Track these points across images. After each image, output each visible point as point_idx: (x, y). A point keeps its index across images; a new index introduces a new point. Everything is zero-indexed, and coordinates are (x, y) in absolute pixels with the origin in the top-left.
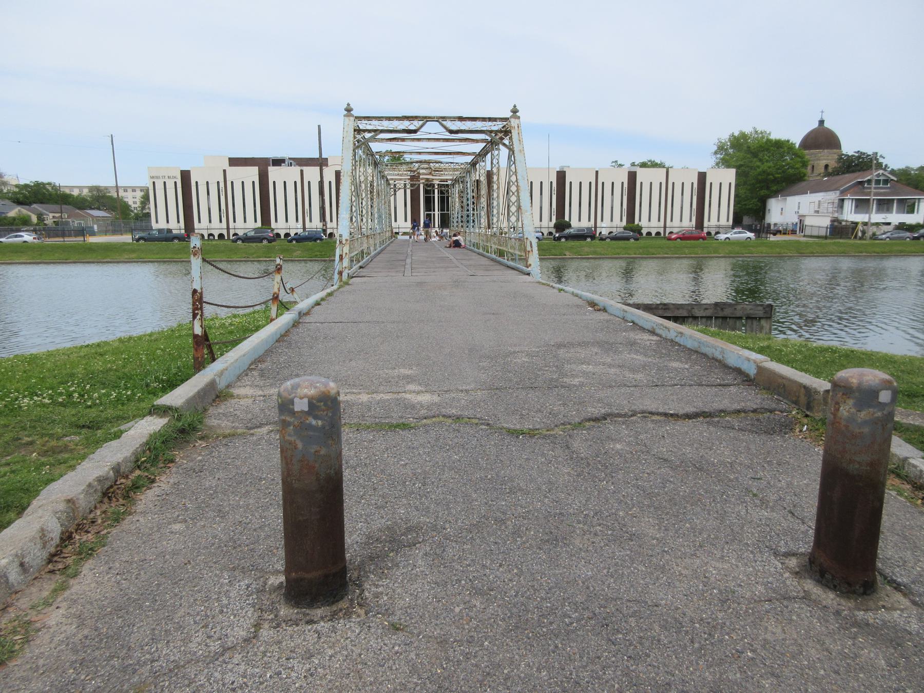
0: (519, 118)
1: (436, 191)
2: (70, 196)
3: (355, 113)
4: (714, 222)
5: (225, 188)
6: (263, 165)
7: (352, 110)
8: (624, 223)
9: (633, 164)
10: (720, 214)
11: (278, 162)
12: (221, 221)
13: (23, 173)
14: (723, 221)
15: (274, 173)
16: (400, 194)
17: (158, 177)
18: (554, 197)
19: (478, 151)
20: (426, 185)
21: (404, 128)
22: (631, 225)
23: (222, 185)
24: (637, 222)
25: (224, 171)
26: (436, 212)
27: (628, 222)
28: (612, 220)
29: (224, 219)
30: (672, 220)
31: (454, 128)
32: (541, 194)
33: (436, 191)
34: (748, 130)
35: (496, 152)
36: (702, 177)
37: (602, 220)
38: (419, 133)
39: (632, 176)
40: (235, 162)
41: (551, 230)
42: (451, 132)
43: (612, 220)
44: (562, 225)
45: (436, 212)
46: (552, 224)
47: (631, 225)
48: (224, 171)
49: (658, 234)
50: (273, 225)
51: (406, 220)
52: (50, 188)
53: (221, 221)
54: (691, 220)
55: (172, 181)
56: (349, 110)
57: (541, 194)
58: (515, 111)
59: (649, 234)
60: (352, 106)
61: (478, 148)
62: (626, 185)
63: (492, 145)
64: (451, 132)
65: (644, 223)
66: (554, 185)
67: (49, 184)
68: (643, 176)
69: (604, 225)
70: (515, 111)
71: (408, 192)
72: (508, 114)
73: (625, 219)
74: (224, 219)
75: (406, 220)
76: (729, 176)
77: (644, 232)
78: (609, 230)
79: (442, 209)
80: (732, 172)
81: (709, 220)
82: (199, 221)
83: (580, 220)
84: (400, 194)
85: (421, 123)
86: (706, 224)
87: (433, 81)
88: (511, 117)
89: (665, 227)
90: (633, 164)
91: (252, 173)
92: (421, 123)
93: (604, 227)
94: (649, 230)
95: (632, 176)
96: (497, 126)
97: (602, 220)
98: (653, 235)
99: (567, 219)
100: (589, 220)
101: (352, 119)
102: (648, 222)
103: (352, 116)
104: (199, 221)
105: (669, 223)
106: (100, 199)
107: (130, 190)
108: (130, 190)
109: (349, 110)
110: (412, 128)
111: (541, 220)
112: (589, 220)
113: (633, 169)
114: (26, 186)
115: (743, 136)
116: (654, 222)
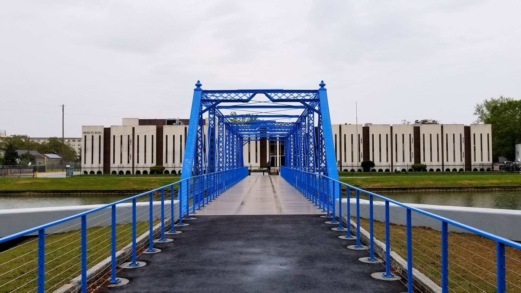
0: (326, 90)
1: (278, 142)
2: (37, 144)
3: (203, 88)
4: (478, 161)
5: (133, 140)
6: (160, 124)
7: (325, 85)
8: (413, 163)
9: (417, 122)
10: (483, 156)
11: (171, 122)
12: (128, 162)
13: (11, 129)
14: (485, 161)
15: (167, 130)
16: (253, 143)
17: (88, 133)
18: (413, 151)
19: (300, 114)
20: (270, 138)
21: (238, 98)
22: (418, 164)
23: (131, 138)
24: (422, 162)
25: (133, 129)
26: (278, 156)
27: (157, 164)
28: (404, 161)
29: (131, 161)
30: (447, 161)
31: (276, 98)
32: (352, 143)
33: (278, 142)
34: (496, 98)
35: (312, 115)
36: (467, 130)
37: (397, 161)
38: (250, 102)
39: (417, 130)
40: (143, 122)
41: (360, 168)
42: (274, 101)
43: (404, 161)
44: (367, 165)
45: (278, 156)
46: (360, 164)
47: (418, 164)
48: (133, 129)
49: (438, 170)
50: (164, 165)
51: (256, 162)
52: (24, 140)
53: (128, 162)
54: (461, 161)
55: (98, 135)
56: (198, 85)
57: (352, 143)
58: (322, 85)
59: (432, 170)
60: (201, 83)
61: (300, 112)
62: (412, 136)
63: (310, 110)
64: (274, 101)
65: (427, 162)
66: (361, 136)
67: (23, 137)
68: (424, 130)
69: (398, 164)
70: (322, 85)
71: (259, 142)
72: (318, 88)
73: (413, 159)
74: (131, 161)
75: (256, 162)
76: (488, 129)
77: (428, 169)
78: (402, 168)
79: (282, 153)
80: (490, 126)
81: (475, 161)
82: (114, 163)
83: (380, 161)
84: (253, 143)
85: (251, 94)
86: (473, 162)
87: (264, 61)
88: (320, 89)
89: (443, 165)
90: (417, 122)
91: (152, 130)
92: (251, 94)
93: (399, 165)
94: (431, 167)
95: (417, 130)
96: (312, 96)
97: (397, 161)
98: (451, 171)
99: (371, 159)
100: (387, 161)
101: (201, 92)
102: (430, 161)
103: (201, 90)
104: (114, 163)
105: (445, 163)
106: (56, 145)
107: (77, 140)
108: (77, 140)
109: (198, 85)
110: (245, 98)
111: (352, 161)
112: (387, 161)
113: (417, 125)
114: (8, 138)
115: (494, 101)
116: (435, 162)
